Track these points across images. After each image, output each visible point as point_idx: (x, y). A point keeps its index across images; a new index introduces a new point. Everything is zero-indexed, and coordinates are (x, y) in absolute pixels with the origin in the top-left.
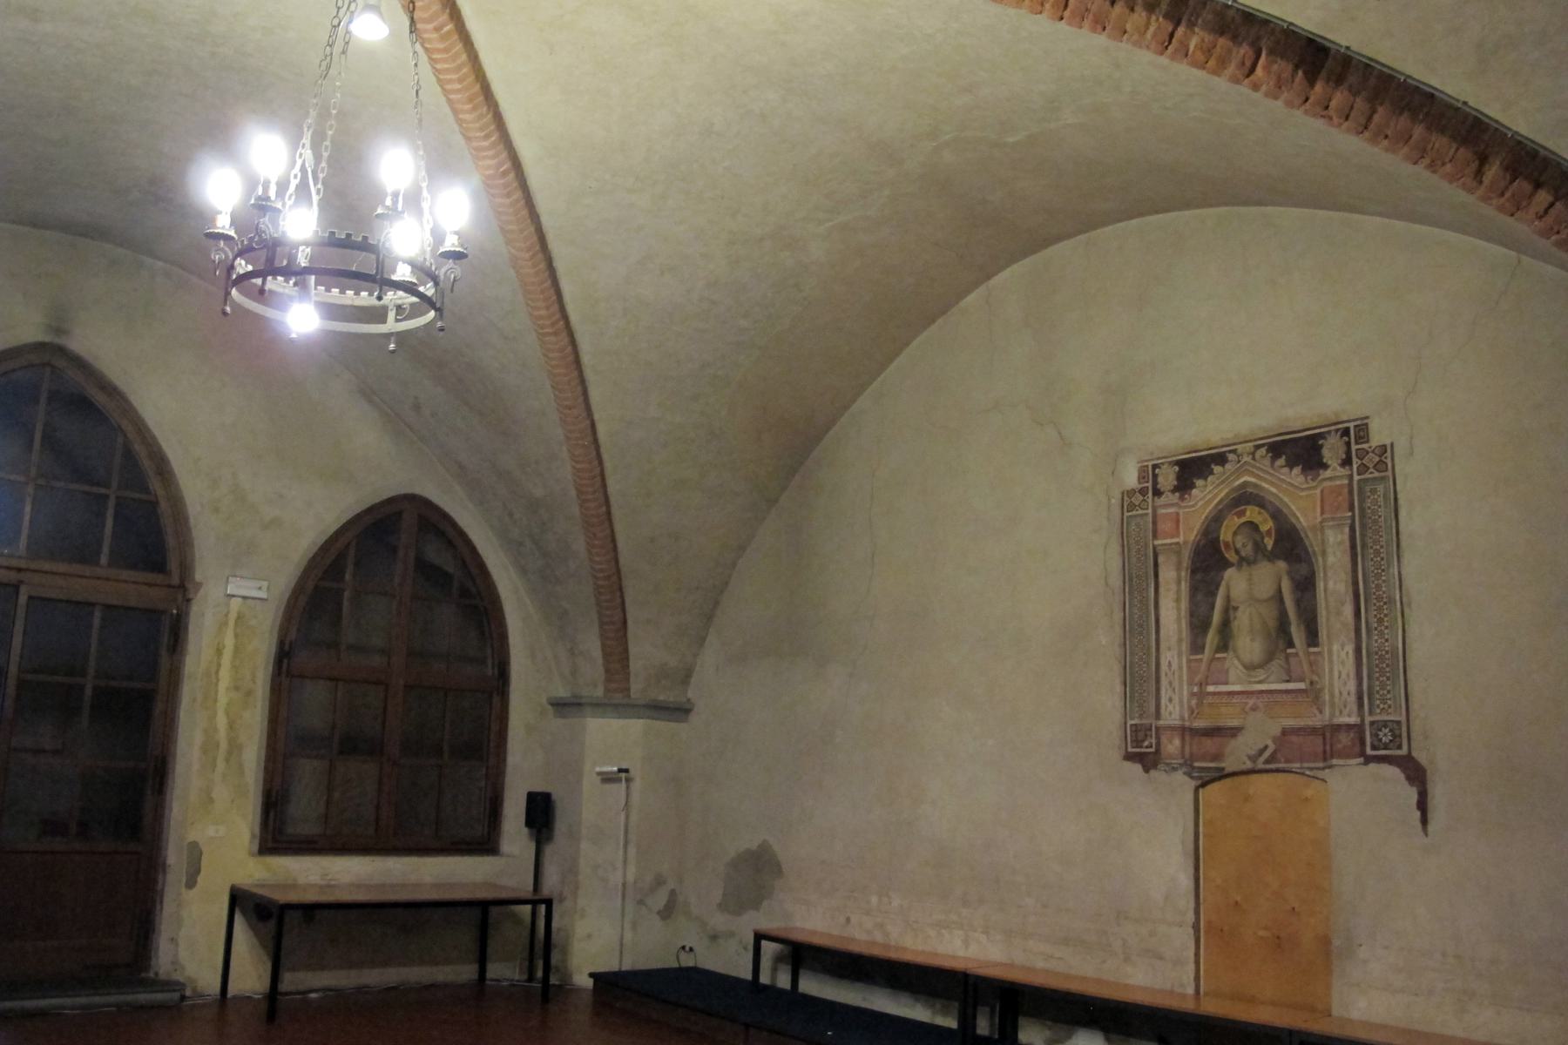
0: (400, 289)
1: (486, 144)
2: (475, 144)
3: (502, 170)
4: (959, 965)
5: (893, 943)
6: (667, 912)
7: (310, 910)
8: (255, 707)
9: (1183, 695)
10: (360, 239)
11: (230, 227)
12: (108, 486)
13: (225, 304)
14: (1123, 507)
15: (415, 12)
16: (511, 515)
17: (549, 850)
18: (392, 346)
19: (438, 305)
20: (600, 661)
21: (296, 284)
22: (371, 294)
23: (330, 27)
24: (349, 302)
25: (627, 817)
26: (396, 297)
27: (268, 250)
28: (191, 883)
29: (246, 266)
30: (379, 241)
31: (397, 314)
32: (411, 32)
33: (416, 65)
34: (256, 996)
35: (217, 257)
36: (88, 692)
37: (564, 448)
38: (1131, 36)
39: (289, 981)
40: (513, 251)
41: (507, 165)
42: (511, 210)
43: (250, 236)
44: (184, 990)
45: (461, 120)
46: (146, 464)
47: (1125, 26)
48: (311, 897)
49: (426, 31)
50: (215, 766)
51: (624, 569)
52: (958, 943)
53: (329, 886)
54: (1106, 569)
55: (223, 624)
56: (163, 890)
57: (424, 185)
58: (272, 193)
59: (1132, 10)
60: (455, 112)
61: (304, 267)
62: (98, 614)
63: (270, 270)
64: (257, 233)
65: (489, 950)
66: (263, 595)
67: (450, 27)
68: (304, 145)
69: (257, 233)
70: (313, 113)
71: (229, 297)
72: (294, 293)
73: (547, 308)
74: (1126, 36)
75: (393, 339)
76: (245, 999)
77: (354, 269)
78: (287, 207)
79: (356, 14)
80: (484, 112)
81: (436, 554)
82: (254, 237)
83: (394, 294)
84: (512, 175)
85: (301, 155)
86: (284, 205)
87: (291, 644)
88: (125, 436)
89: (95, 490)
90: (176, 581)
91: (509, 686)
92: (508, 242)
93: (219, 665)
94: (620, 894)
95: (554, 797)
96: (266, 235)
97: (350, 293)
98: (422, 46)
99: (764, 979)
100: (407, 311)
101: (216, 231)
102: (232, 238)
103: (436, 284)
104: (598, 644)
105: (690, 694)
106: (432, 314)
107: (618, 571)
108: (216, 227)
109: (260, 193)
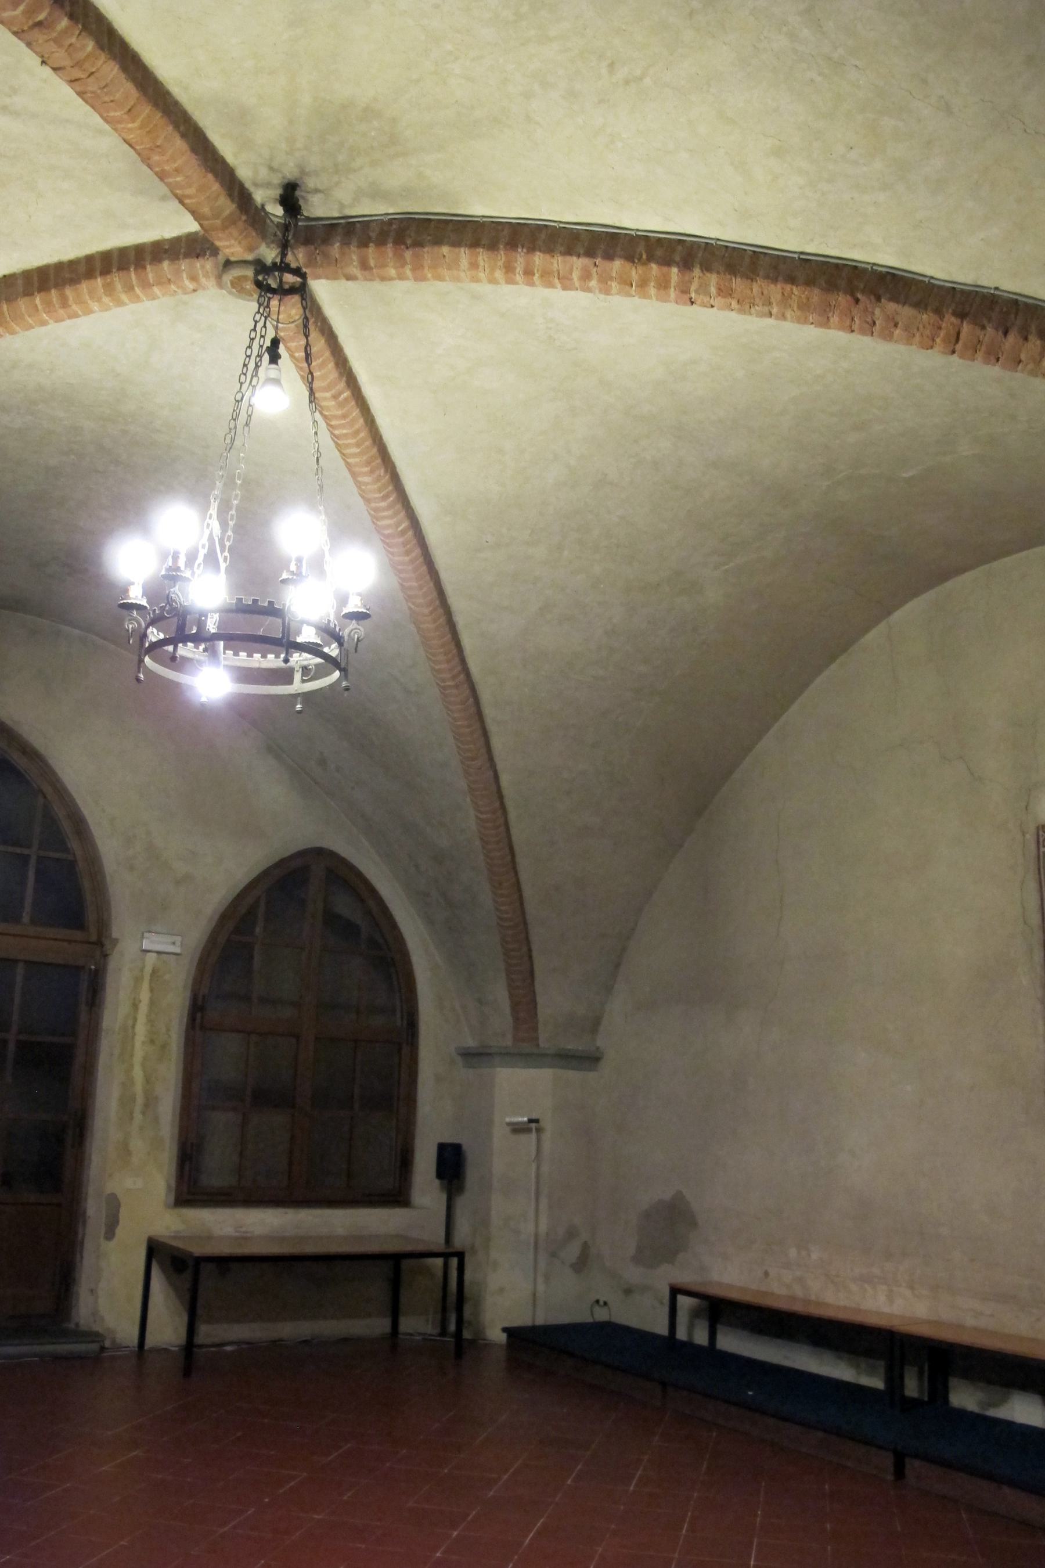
0: (305, 651)
1: (383, 504)
2: (373, 505)
3: (400, 529)
4: (882, 1322)
5: (813, 1298)
6: (581, 1264)
7: (223, 1263)
8: (170, 1060)
9: (340, 425)
10: (266, 604)
11: (142, 597)
12: (29, 847)
13: (139, 672)
14: (1038, 842)
15: (314, 382)
16: (417, 866)
17: (461, 1203)
18: (299, 706)
19: (343, 665)
20: (507, 1010)
21: (205, 650)
22: (277, 656)
23: (247, 416)
24: (256, 665)
25: (538, 1168)
26: (301, 658)
27: (179, 620)
28: (110, 1234)
29: (158, 634)
30: (284, 605)
31: (303, 675)
32: (311, 402)
33: (316, 433)
34: (173, 1349)
35: (131, 626)
36: (12, 1047)
37: (468, 800)
38: (1027, 365)
39: (206, 1333)
40: (413, 607)
41: (405, 524)
42: (410, 568)
43: (162, 605)
44: (103, 1341)
45: (360, 482)
46: (66, 826)
47: (1019, 356)
48: (226, 1250)
49: (325, 399)
50: (131, 1118)
51: (529, 918)
52: (882, 1298)
53: (245, 1238)
54: (1024, 908)
55: (138, 980)
56: (83, 1239)
57: (326, 549)
58: (181, 563)
59: (1026, 339)
60: (354, 475)
61: (213, 633)
62: (20, 970)
63: (181, 636)
64: (168, 602)
65: (403, 1299)
66: (178, 950)
67: (347, 394)
68: (211, 515)
69: (168, 602)
70: (219, 484)
71: (142, 665)
72: (202, 658)
73: (448, 662)
74: (1020, 367)
75: (299, 699)
76: (162, 1351)
77: (261, 634)
78: (196, 575)
79: (257, 388)
80: (382, 474)
81: (344, 906)
82: (165, 606)
83: (300, 656)
84: (410, 533)
85: (208, 525)
86: (193, 574)
87: (204, 996)
88: (45, 797)
89: (18, 850)
90: (94, 938)
91: (418, 1037)
92: (409, 598)
93: (135, 1019)
94: (532, 1247)
95: (465, 1147)
96: (176, 603)
97: (257, 656)
98: (321, 413)
99: (681, 1334)
100: (312, 673)
101: (130, 601)
102: (146, 607)
103: (341, 644)
104: (506, 994)
105: (599, 1043)
106: (337, 674)
107: (525, 923)
108: (128, 597)
109: (170, 564)
